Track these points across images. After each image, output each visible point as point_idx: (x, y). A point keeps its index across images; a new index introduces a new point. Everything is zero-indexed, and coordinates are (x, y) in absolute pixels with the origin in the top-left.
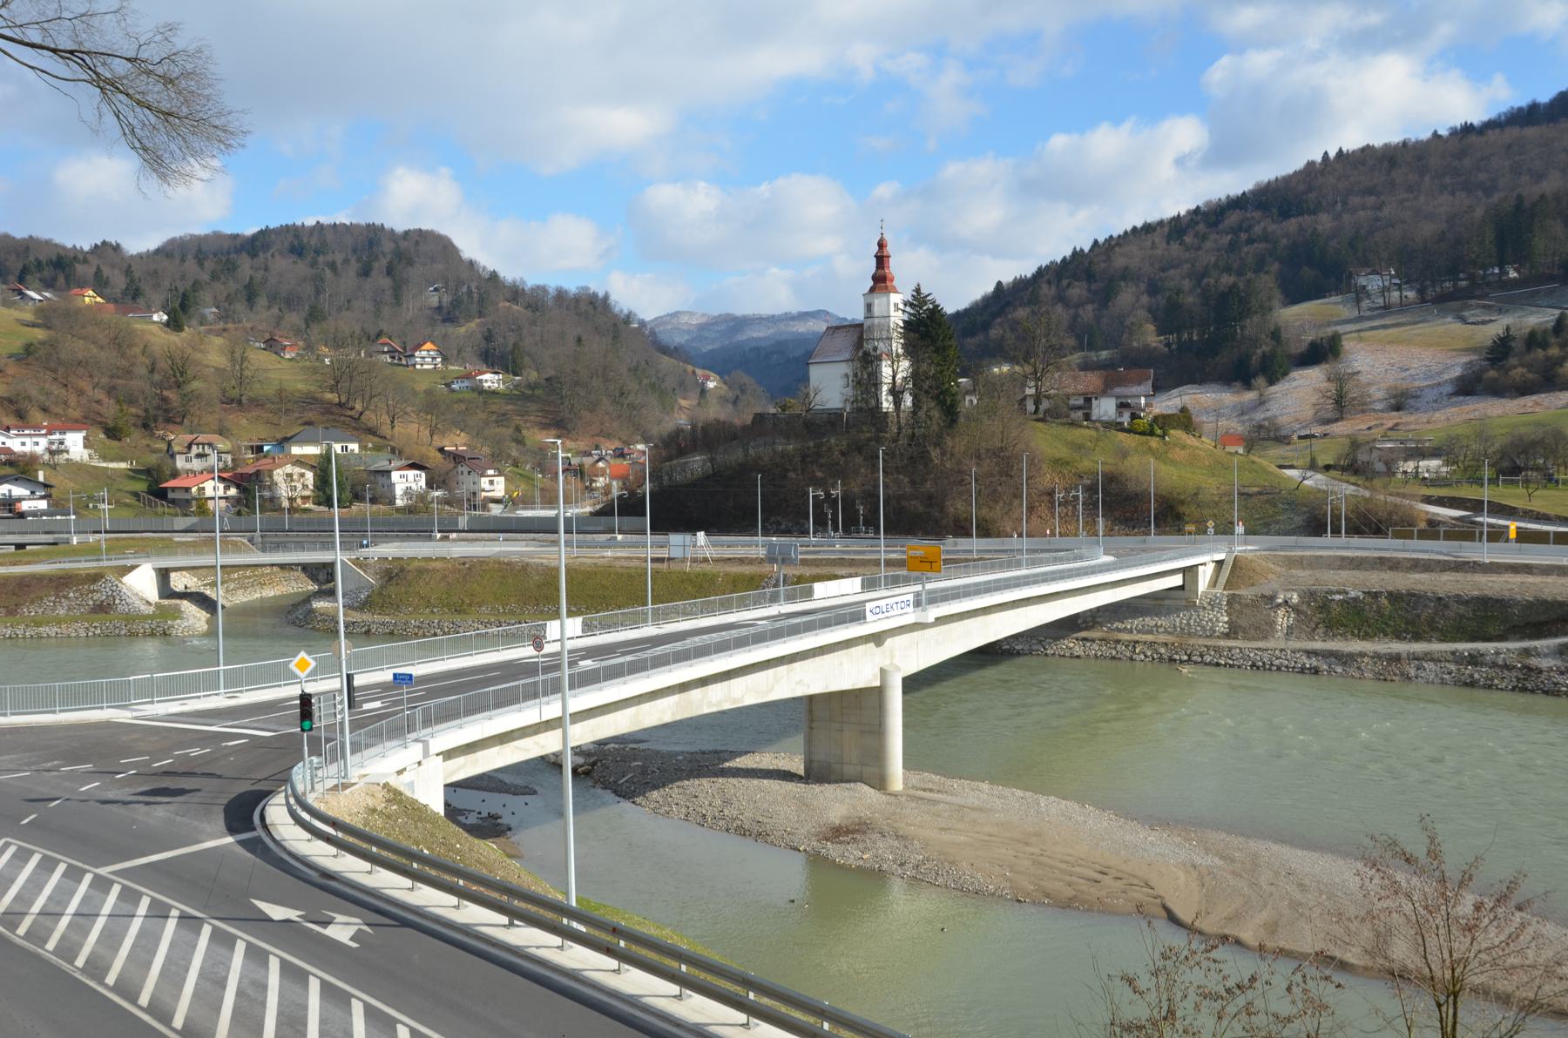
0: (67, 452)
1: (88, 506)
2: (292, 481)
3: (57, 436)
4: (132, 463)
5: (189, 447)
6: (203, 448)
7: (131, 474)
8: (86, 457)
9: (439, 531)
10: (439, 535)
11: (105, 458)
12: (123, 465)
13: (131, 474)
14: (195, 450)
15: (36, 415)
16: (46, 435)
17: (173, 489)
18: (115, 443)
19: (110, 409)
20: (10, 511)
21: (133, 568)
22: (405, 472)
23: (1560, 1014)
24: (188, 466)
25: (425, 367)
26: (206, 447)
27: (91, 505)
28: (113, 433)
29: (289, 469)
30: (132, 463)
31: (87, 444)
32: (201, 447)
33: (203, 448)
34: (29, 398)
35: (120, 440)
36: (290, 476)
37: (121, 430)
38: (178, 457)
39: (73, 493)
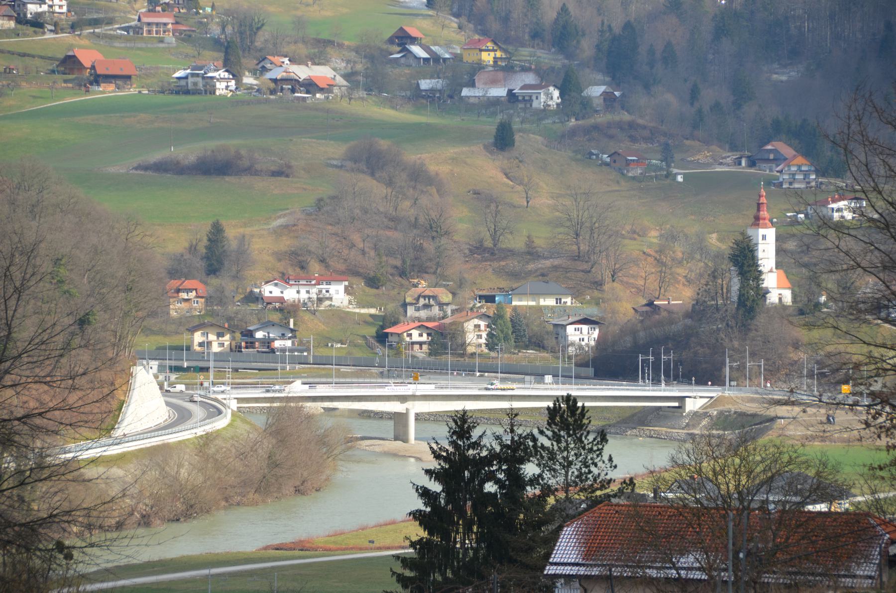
0: (330, 299)
1: (328, 345)
2: (480, 330)
3: (324, 287)
4: (380, 309)
5: (418, 299)
6: (429, 300)
7: (371, 320)
8: (346, 302)
9: (479, 371)
10: (478, 374)
11: (361, 305)
12: (373, 311)
13: (371, 320)
14: (422, 302)
15: (315, 267)
16: (315, 285)
17: (392, 334)
18: (374, 291)
19: (370, 263)
20: (268, 347)
21: (292, 382)
22: (580, 326)
23: (737, 592)
24: (417, 314)
25: (796, 186)
26: (431, 300)
27: (330, 345)
28: (373, 282)
29: (476, 321)
30: (380, 309)
31: (347, 291)
32: (427, 299)
33: (429, 300)
34: (309, 252)
35: (377, 288)
36: (477, 326)
37: (379, 280)
38: (408, 307)
39: (207, 369)
